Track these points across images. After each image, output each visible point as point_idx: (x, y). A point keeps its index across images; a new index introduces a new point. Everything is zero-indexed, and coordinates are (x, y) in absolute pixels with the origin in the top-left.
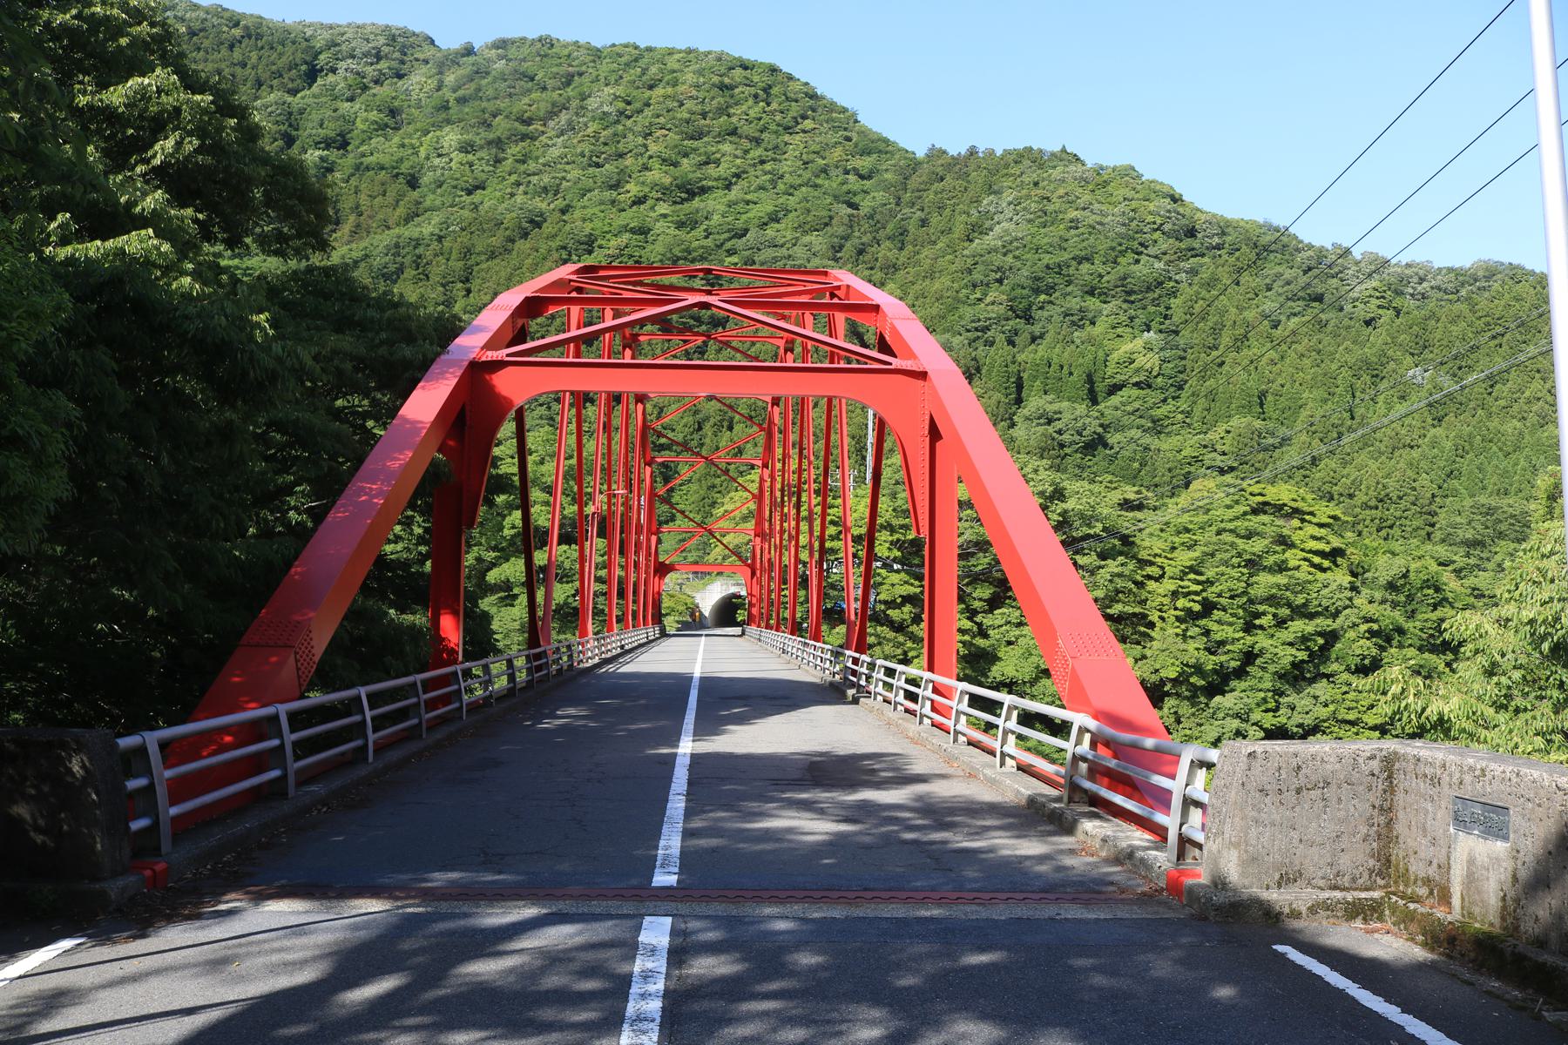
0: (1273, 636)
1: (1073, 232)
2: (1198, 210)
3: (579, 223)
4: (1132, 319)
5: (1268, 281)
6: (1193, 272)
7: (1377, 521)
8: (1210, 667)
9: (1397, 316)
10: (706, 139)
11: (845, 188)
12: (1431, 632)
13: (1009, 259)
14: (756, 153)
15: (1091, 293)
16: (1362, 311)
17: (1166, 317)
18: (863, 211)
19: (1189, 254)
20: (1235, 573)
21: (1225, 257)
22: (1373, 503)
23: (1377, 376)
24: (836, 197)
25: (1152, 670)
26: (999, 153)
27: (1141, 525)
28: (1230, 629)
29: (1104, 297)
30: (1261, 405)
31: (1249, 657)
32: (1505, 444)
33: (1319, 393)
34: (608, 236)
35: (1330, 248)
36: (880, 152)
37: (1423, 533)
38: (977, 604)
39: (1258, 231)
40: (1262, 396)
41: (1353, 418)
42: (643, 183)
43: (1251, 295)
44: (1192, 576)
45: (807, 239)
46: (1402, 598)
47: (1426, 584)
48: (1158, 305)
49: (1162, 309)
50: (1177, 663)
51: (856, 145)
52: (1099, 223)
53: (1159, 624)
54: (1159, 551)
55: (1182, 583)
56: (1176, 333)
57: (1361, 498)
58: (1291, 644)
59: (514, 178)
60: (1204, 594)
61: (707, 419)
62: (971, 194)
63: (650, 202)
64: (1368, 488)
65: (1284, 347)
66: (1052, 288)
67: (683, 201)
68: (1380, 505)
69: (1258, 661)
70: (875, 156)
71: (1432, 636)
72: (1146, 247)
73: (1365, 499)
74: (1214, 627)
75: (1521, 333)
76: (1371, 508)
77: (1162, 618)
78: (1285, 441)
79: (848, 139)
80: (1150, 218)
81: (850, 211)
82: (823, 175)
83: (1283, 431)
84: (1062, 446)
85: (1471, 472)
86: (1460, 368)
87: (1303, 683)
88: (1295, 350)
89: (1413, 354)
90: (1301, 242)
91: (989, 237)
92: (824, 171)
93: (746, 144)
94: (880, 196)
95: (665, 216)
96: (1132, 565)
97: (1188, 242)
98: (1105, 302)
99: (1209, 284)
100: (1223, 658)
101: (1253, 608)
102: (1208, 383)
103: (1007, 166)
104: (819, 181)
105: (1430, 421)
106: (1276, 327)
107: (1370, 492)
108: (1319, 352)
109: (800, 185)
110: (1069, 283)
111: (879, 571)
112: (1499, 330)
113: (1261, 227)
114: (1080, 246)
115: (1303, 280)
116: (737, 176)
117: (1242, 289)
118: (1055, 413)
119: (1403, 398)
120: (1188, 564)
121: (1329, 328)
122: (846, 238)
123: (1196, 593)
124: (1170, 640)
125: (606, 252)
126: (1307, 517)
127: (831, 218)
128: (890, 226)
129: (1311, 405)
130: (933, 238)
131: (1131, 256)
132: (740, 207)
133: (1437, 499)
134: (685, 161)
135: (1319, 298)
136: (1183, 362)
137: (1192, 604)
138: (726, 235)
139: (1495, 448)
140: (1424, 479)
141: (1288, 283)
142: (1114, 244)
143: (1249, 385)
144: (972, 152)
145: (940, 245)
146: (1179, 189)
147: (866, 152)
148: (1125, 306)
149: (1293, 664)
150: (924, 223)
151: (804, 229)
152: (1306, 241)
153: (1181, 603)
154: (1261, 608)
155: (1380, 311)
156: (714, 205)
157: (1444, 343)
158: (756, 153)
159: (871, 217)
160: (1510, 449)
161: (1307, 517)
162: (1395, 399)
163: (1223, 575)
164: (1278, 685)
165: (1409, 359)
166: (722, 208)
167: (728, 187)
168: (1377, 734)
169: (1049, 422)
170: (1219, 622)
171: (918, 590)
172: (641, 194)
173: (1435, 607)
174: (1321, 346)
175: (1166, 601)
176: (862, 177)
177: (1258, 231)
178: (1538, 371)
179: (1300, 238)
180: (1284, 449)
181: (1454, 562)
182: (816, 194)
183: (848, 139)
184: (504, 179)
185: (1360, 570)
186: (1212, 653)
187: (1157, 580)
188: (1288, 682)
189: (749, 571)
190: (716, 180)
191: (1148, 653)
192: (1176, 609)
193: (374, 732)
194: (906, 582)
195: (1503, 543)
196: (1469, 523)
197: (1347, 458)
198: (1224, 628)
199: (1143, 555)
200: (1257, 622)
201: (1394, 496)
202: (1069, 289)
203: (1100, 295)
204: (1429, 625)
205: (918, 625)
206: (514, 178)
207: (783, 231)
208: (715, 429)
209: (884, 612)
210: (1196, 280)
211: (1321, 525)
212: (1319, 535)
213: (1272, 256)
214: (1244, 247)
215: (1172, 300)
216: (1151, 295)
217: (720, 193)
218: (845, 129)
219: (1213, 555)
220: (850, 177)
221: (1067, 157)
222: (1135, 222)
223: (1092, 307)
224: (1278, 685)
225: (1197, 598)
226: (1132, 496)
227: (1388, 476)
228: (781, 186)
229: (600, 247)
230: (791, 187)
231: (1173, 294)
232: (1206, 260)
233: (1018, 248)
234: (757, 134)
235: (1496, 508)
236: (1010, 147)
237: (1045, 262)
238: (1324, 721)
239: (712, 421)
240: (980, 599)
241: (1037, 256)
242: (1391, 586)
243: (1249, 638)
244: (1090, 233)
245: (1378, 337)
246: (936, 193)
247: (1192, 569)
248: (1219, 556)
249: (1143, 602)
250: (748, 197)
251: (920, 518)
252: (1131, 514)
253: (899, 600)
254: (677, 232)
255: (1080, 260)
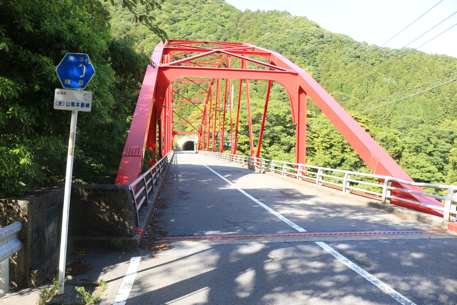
0: (349, 154)
1: (288, 35)
2: (324, 30)
3: (141, 30)
4: (305, 62)
5: (344, 52)
6: (322, 48)
7: (374, 122)
8: (332, 163)
9: (381, 63)
10: (179, 5)
11: (221, 21)
12: (393, 153)
13: (269, 43)
14: (194, 9)
15: (293, 54)
16: (371, 61)
17: (314, 61)
18: (226, 28)
19: (322, 43)
20: (339, 136)
21: (332, 44)
22: (373, 117)
23: (374, 80)
24: (218, 24)
25: (316, 164)
26: (266, 11)
27: (312, 122)
28: (337, 152)
29: (297, 55)
30: (342, 88)
31: (343, 160)
32: (410, 100)
33: (358, 84)
34: (150, 34)
35: (362, 42)
36: (231, 10)
37: (387, 125)
38: (266, 144)
39: (342, 37)
40: (342, 85)
41: (367, 92)
42: (160, 18)
43: (339, 56)
44: (327, 137)
45: (209, 36)
46: (385, 144)
47: (392, 140)
48: (312, 58)
49: (313, 59)
50: (323, 162)
51: (224, 8)
52: (296, 33)
53: (318, 150)
54: (318, 130)
55: (324, 139)
56: (317, 66)
57: (370, 115)
58: (354, 157)
59: (121, 15)
60: (330, 142)
61: (181, 89)
62: (258, 23)
63: (162, 24)
64: (372, 112)
65: (348, 71)
66: (282, 52)
67: (172, 23)
68: (375, 117)
69: (345, 161)
70: (230, 11)
71: (393, 155)
72: (309, 41)
73: (371, 115)
74: (333, 151)
75: (415, 69)
76: (372, 118)
77: (319, 149)
78: (348, 98)
79: (222, 6)
80: (310, 32)
81: (222, 28)
82: (214, 17)
83: (347, 95)
84: (284, 99)
85: (400, 108)
86: (398, 78)
87: (357, 168)
88: (352, 72)
89: (385, 74)
90: (354, 40)
91: (263, 37)
92: (214, 15)
93: (191, 7)
94: (231, 23)
95: (167, 28)
96: (310, 133)
97: (321, 39)
98: (297, 57)
99: (327, 52)
100: (336, 160)
101: (344, 146)
102: (326, 81)
103: (269, 15)
104: (213, 19)
105: (389, 93)
106: (346, 65)
107: (372, 114)
108: (358, 73)
109: (207, 20)
110: (287, 51)
111: (338, 131)
112: (409, 67)
113: (342, 35)
114: (290, 40)
115: (354, 51)
116: (189, 16)
117: (336, 54)
118: (283, 89)
119: (382, 86)
120: (326, 133)
121: (361, 65)
122: (221, 36)
123: (328, 142)
124: (321, 155)
125: (149, 38)
126: (359, 120)
127: (217, 30)
128: (234, 33)
129: (356, 88)
130: (247, 36)
131: (305, 43)
132: (190, 26)
133: (391, 116)
134: (173, 11)
135: (359, 57)
136: (319, 75)
137: (327, 145)
138: (185, 34)
139: (407, 101)
140: (387, 110)
141: (350, 52)
142: (300, 40)
143: (338, 82)
144: (258, 11)
145: (249, 39)
146: (319, 24)
147: (227, 10)
148: (303, 58)
149: (355, 163)
150: (244, 32)
151: (209, 33)
152: (355, 40)
153: (324, 144)
154: (346, 146)
155: (376, 61)
156: (182, 25)
157: (394, 71)
158: (194, 9)
159: (228, 30)
160: (411, 102)
161: (359, 120)
162: (380, 87)
163: (336, 136)
164: (351, 168)
165: (384, 75)
166: (184, 26)
167: (186, 20)
168: (378, 182)
169: (281, 92)
170: (334, 150)
171: (249, 140)
172: (160, 21)
173: (394, 146)
174: (359, 71)
175: (320, 144)
176: (226, 18)
177: (341, 37)
178: (419, 80)
179: (353, 39)
180: (348, 100)
181: (398, 133)
182: (212, 22)
183: (222, 6)
184: (118, 16)
185: (374, 136)
186: (332, 159)
187: (317, 138)
188: (353, 167)
189: (199, 134)
190: (182, 17)
191: (314, 159)
192: (322, 146)
193: (146, 182)
194: (246, 138)
195: (411, 129)
196: (402, 123)
197: (366, 103)
198: (336, 151)
199: (313, 130)
200: (345, 150)
201: (379, 115)
202: (287, 52)
203: (296, 54)
204: (392, 151)
205: (249, 150)
206: (121, 15)
207: (202, 33)
208: (183, 92)
209: (239, 146)
210: (323, 51)
211: (363, 123)
212: (362, 126)
213: (345, 44)
214: (337, 41)
215: (316, 56)
216: (310, 55)
217: (183, 21)
218: (221, 3)
219: (333, 131)
220: (222, 17)
221: (286, 13)
222: (306, 33)
223: (293, 58)
224: (351, 168)
225: (328, 143)
226: (309, 113)
227: (377, 109)
228: (202, 20)
229: (148, 37)
230: (205, 20)
231: (317, 54)
232: (326, 45)
233: (272, 40)
234: (194, 4)
235: (410, 119)
236: (269, 10)
237: (280, 44)
238: (363, 179)
239: (182, 90)
240: (267, 143)
241: (277, 43)
242: (382, 140)
243: (343, 155)
244: (293, 36)
245: (375, 69)
246: (248, 23)
247: (327, 135)
248: (335, 131)
249: (313, 144)
250: (192, 23)
251: (295, 118)
252: (309, 119)
253: (244, 143)
254: (171, 33)
255: (290, 44)
